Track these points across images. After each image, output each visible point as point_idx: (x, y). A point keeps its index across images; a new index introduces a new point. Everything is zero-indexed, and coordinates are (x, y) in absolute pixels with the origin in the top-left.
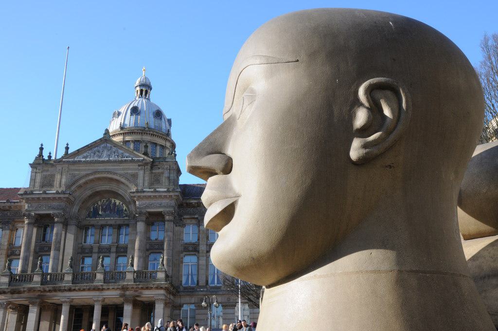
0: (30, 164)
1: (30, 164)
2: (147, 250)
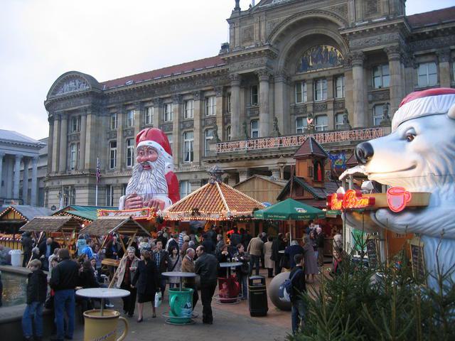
0: (227, 20)
1: (227, 20)
2: (370, 102)
